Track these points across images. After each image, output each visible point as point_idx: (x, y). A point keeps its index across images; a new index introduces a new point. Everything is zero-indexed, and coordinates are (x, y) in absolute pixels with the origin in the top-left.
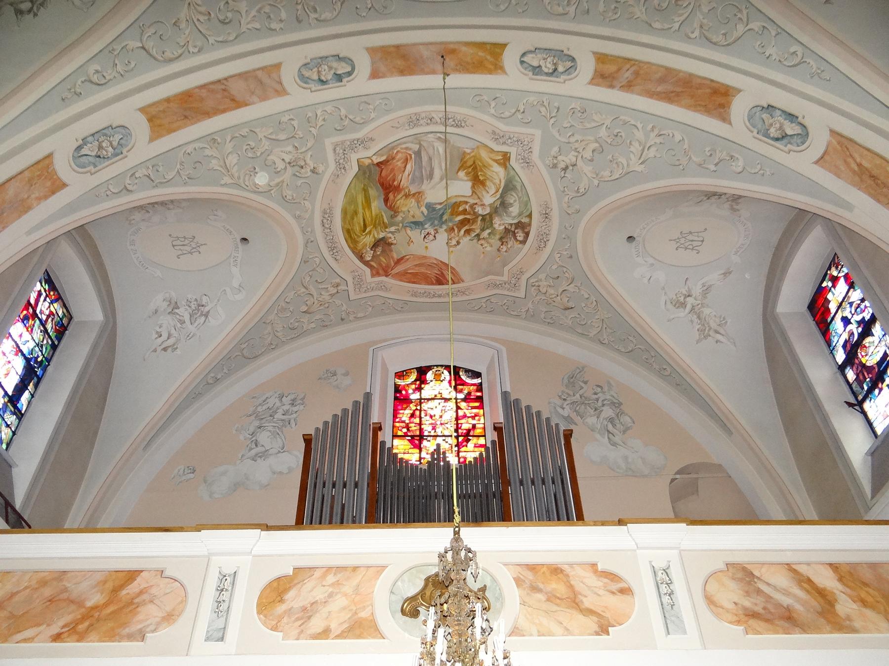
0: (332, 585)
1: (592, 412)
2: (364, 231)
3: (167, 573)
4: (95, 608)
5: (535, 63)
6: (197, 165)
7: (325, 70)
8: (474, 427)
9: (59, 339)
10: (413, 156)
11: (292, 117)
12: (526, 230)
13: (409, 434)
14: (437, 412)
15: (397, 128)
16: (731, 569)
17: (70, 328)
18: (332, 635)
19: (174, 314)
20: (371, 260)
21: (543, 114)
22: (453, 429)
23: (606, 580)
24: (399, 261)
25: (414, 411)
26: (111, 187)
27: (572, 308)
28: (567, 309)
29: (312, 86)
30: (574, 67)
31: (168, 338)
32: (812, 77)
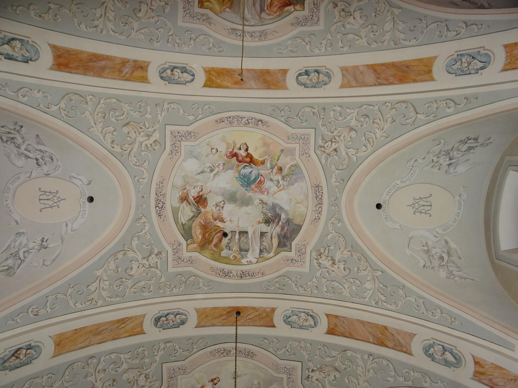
5: (185, 74)
6: (412, 29)
7: (315, 79)
10: (266, 8)
11: (342, 49)
15: (275, 31)
21: (178, 38)
26: (476, 30)
29: (324, 70)
30: (161, 73)
32: (7, 84)
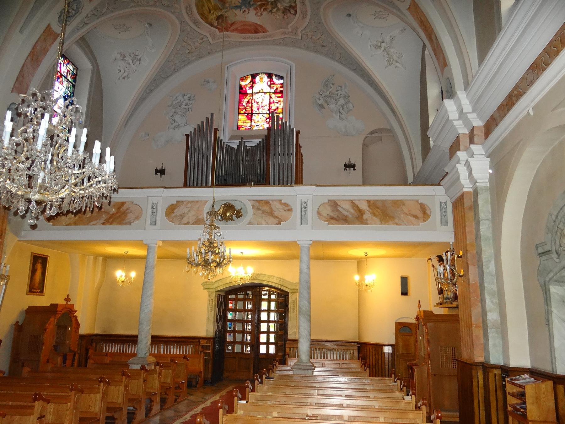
0: (190, 207)
1: (334, 101)
2: (210, 12)
3: (135, 203)
4: (113, 214)
8: (278, 108)
9: (75, 81)
12: (295, 9)
13: (246, 112)
14: (259, 100)
16: (330, 202)
17: (78, 74)
18: (190, 224)
19: (124, 60)
20: (218, 25)
22: (267, 109)
23: (284, 206)
24: (232, 24)
25: (249, 100)
27: (325, 46)
28: (323, 46)
31: (124, 73)
